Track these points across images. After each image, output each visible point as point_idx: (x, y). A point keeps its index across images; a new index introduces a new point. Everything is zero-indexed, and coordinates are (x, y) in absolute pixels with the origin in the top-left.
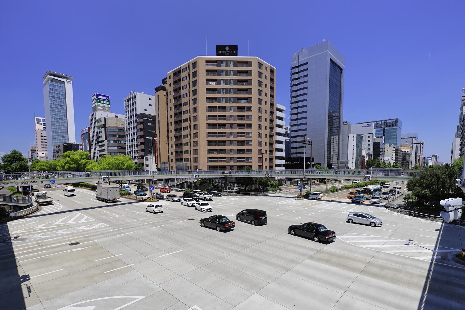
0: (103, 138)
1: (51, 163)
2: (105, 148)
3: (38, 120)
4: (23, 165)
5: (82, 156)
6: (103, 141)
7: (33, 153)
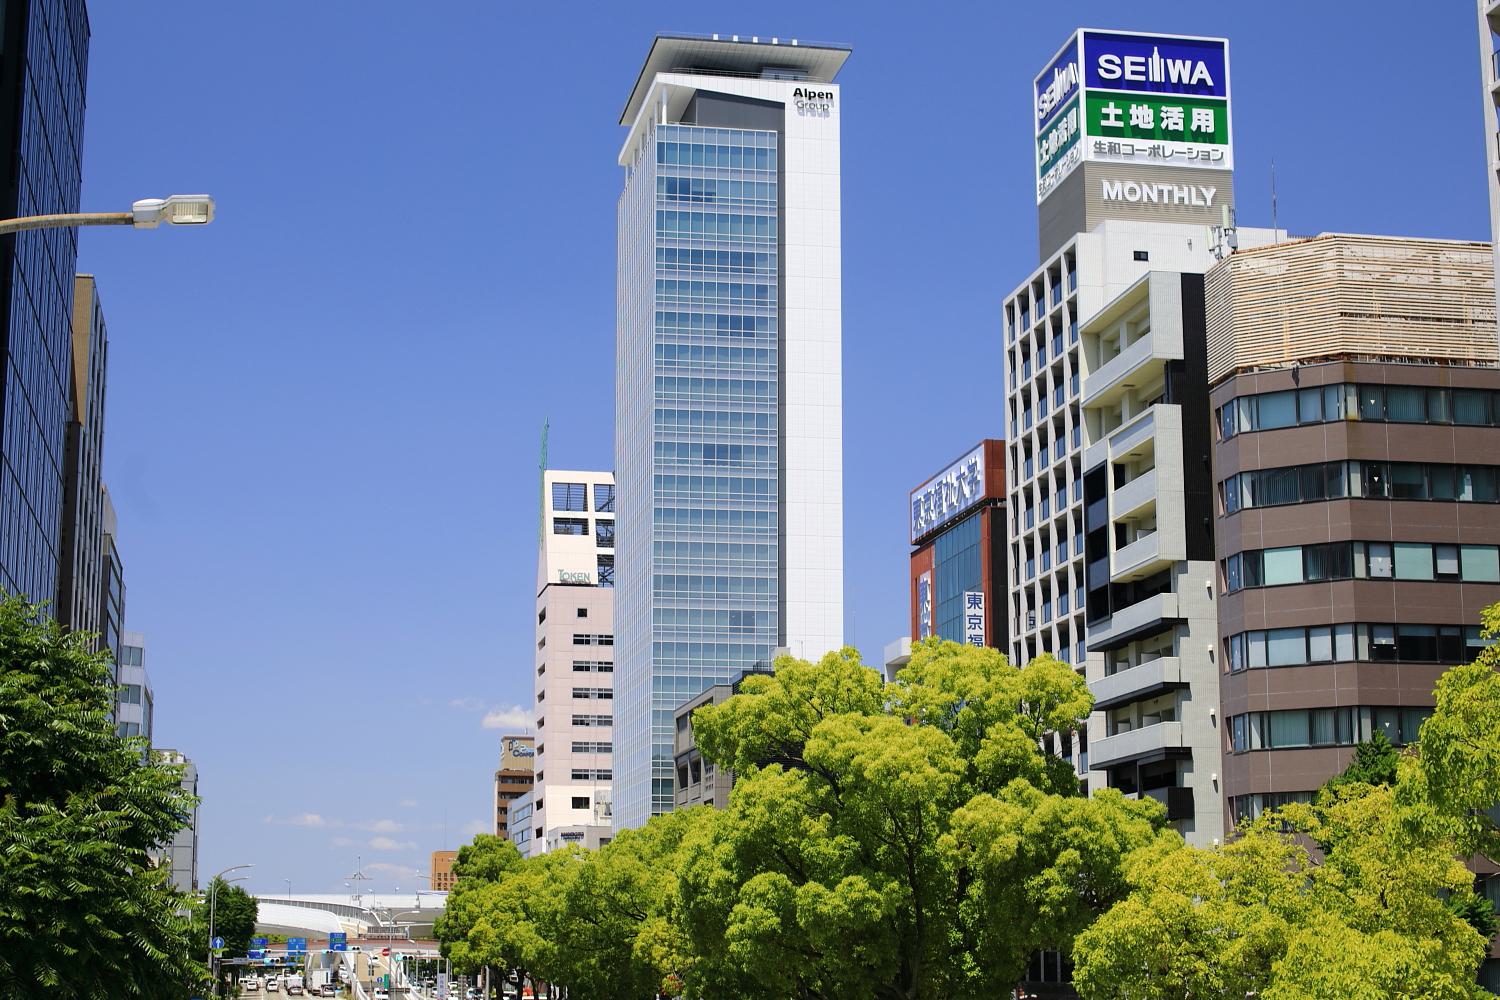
0: (1168, 540)
1: (587, 877)
2: (1193, 661)
3: (570, 495)
4: (56, 874)
5: (972, 735)
6: (1158, 581)
7: (514, 805)
